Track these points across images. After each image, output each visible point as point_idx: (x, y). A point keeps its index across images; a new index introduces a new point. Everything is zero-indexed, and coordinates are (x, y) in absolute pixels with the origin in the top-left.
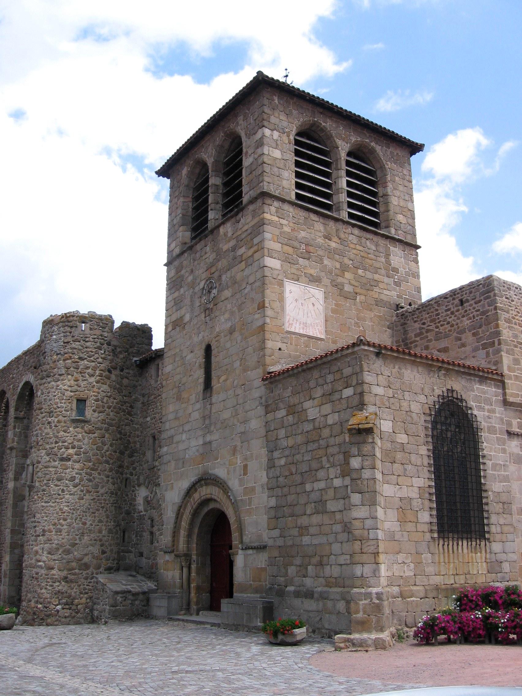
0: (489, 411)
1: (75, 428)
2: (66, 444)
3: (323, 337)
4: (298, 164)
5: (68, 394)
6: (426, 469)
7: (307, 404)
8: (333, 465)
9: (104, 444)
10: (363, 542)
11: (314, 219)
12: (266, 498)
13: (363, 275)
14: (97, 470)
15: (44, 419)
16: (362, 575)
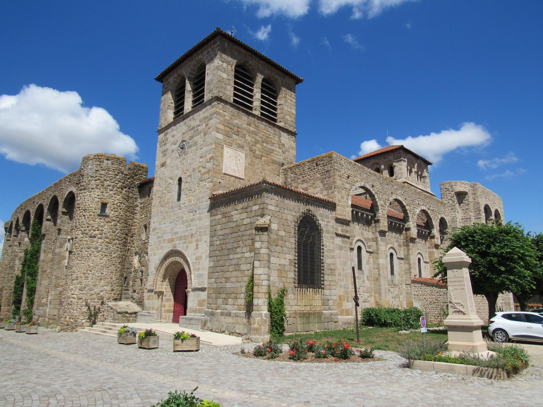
0: (327, 222)
2: (94, 228)
3: (243, 178)
4: (236, 83)
6: (293, 250)
8: (246, 246)
10: (259, 286)
12: (208, 262)
13: (266, 146)
15: (81, 213)
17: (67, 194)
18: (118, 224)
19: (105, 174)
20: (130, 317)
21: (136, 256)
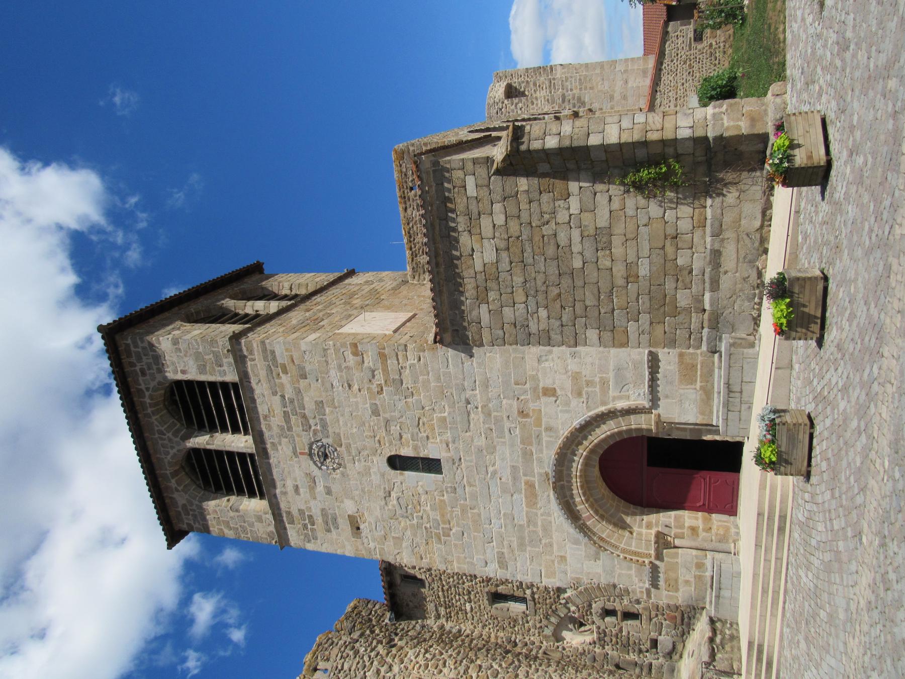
16: (690, 127)
18: (479, 662)
20: (722, 632)
21: (563, 639)
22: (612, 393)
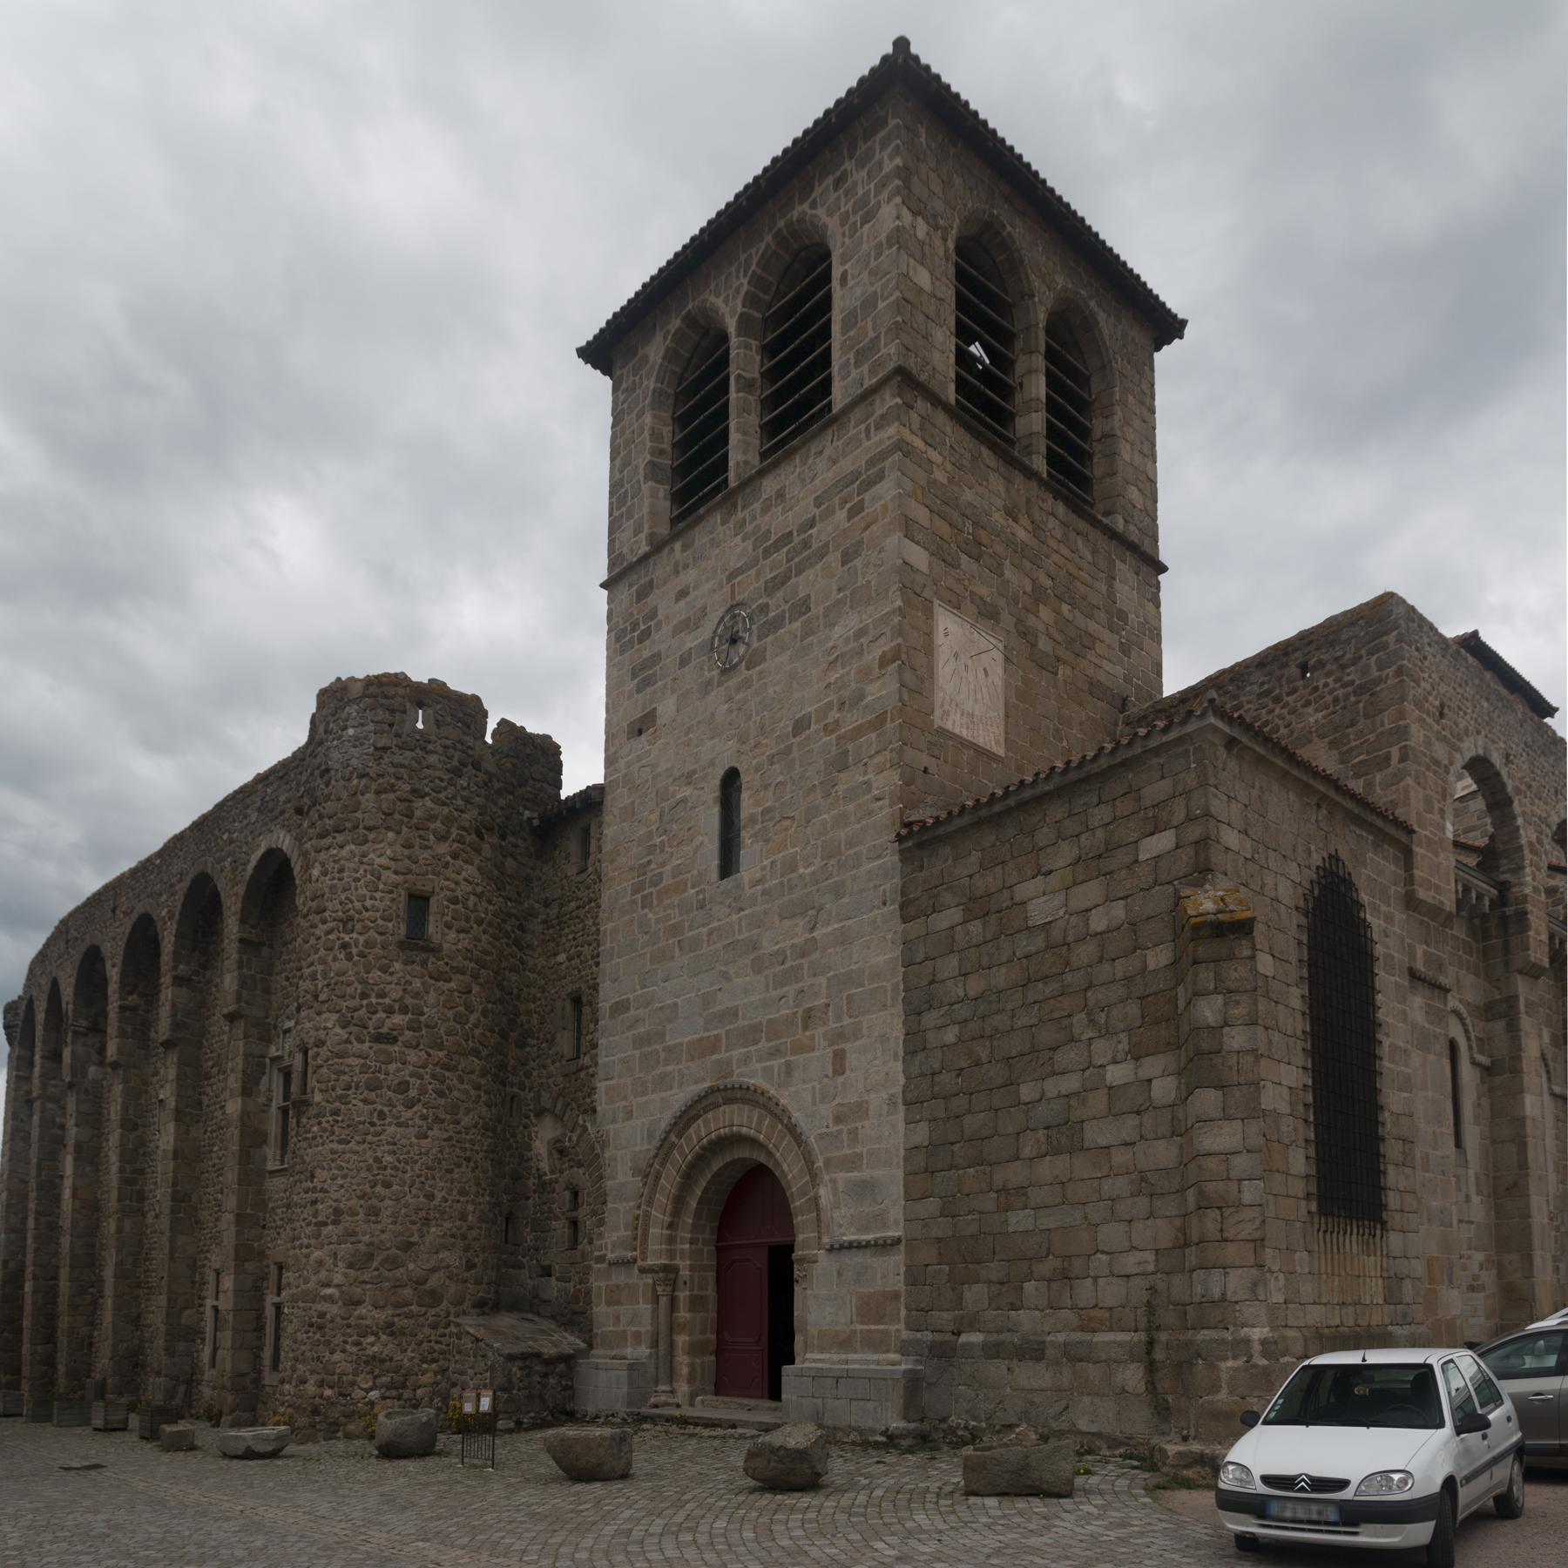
1: (406, 963)
2: (387, 1001)
3: (1001, 752)
5: (388, 876)
7: (1026, 890)
8: (1106, 1033)
9: (470, 1009)
11: (987, 461)
12: (901, 1125)
14: (455, 1069)
15: (332, 937)
16: (1224, 1294)
17: (253, 862)
19: (415, 764)
22: (842, 1176)
